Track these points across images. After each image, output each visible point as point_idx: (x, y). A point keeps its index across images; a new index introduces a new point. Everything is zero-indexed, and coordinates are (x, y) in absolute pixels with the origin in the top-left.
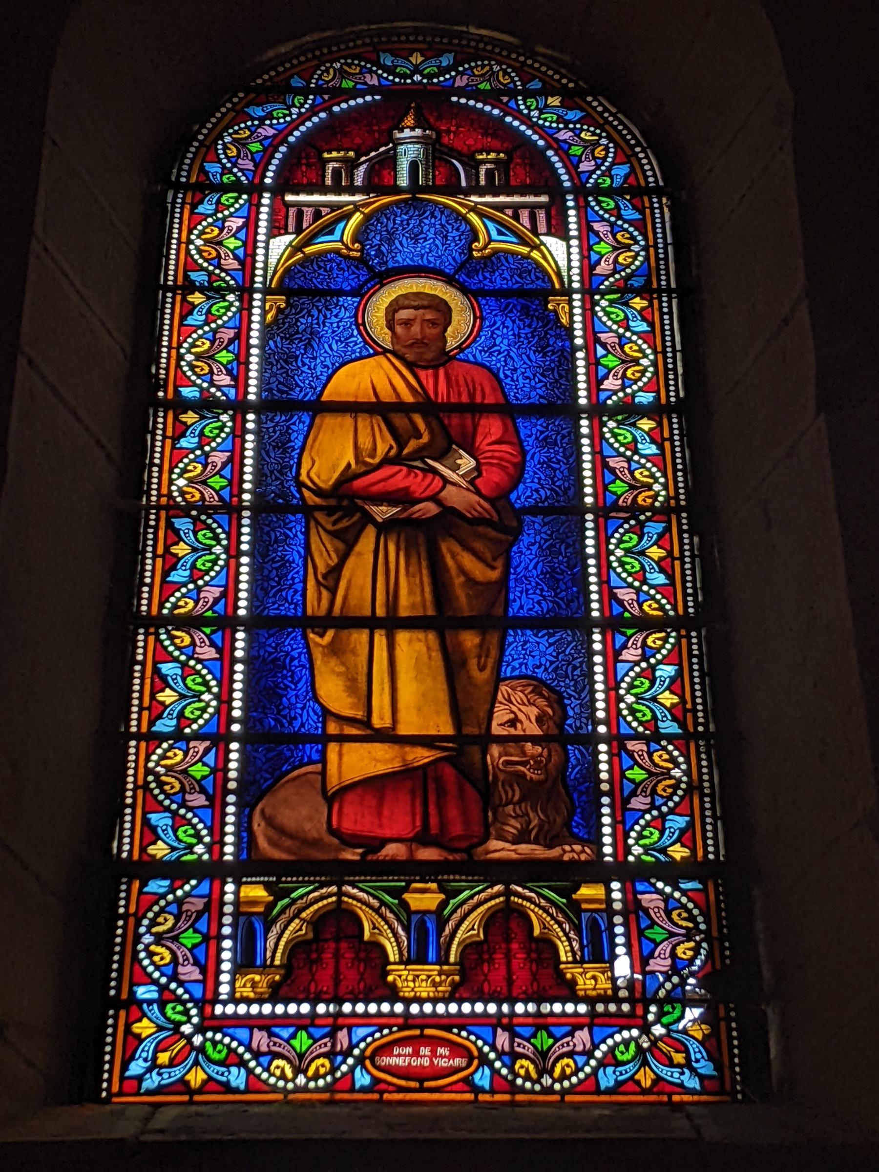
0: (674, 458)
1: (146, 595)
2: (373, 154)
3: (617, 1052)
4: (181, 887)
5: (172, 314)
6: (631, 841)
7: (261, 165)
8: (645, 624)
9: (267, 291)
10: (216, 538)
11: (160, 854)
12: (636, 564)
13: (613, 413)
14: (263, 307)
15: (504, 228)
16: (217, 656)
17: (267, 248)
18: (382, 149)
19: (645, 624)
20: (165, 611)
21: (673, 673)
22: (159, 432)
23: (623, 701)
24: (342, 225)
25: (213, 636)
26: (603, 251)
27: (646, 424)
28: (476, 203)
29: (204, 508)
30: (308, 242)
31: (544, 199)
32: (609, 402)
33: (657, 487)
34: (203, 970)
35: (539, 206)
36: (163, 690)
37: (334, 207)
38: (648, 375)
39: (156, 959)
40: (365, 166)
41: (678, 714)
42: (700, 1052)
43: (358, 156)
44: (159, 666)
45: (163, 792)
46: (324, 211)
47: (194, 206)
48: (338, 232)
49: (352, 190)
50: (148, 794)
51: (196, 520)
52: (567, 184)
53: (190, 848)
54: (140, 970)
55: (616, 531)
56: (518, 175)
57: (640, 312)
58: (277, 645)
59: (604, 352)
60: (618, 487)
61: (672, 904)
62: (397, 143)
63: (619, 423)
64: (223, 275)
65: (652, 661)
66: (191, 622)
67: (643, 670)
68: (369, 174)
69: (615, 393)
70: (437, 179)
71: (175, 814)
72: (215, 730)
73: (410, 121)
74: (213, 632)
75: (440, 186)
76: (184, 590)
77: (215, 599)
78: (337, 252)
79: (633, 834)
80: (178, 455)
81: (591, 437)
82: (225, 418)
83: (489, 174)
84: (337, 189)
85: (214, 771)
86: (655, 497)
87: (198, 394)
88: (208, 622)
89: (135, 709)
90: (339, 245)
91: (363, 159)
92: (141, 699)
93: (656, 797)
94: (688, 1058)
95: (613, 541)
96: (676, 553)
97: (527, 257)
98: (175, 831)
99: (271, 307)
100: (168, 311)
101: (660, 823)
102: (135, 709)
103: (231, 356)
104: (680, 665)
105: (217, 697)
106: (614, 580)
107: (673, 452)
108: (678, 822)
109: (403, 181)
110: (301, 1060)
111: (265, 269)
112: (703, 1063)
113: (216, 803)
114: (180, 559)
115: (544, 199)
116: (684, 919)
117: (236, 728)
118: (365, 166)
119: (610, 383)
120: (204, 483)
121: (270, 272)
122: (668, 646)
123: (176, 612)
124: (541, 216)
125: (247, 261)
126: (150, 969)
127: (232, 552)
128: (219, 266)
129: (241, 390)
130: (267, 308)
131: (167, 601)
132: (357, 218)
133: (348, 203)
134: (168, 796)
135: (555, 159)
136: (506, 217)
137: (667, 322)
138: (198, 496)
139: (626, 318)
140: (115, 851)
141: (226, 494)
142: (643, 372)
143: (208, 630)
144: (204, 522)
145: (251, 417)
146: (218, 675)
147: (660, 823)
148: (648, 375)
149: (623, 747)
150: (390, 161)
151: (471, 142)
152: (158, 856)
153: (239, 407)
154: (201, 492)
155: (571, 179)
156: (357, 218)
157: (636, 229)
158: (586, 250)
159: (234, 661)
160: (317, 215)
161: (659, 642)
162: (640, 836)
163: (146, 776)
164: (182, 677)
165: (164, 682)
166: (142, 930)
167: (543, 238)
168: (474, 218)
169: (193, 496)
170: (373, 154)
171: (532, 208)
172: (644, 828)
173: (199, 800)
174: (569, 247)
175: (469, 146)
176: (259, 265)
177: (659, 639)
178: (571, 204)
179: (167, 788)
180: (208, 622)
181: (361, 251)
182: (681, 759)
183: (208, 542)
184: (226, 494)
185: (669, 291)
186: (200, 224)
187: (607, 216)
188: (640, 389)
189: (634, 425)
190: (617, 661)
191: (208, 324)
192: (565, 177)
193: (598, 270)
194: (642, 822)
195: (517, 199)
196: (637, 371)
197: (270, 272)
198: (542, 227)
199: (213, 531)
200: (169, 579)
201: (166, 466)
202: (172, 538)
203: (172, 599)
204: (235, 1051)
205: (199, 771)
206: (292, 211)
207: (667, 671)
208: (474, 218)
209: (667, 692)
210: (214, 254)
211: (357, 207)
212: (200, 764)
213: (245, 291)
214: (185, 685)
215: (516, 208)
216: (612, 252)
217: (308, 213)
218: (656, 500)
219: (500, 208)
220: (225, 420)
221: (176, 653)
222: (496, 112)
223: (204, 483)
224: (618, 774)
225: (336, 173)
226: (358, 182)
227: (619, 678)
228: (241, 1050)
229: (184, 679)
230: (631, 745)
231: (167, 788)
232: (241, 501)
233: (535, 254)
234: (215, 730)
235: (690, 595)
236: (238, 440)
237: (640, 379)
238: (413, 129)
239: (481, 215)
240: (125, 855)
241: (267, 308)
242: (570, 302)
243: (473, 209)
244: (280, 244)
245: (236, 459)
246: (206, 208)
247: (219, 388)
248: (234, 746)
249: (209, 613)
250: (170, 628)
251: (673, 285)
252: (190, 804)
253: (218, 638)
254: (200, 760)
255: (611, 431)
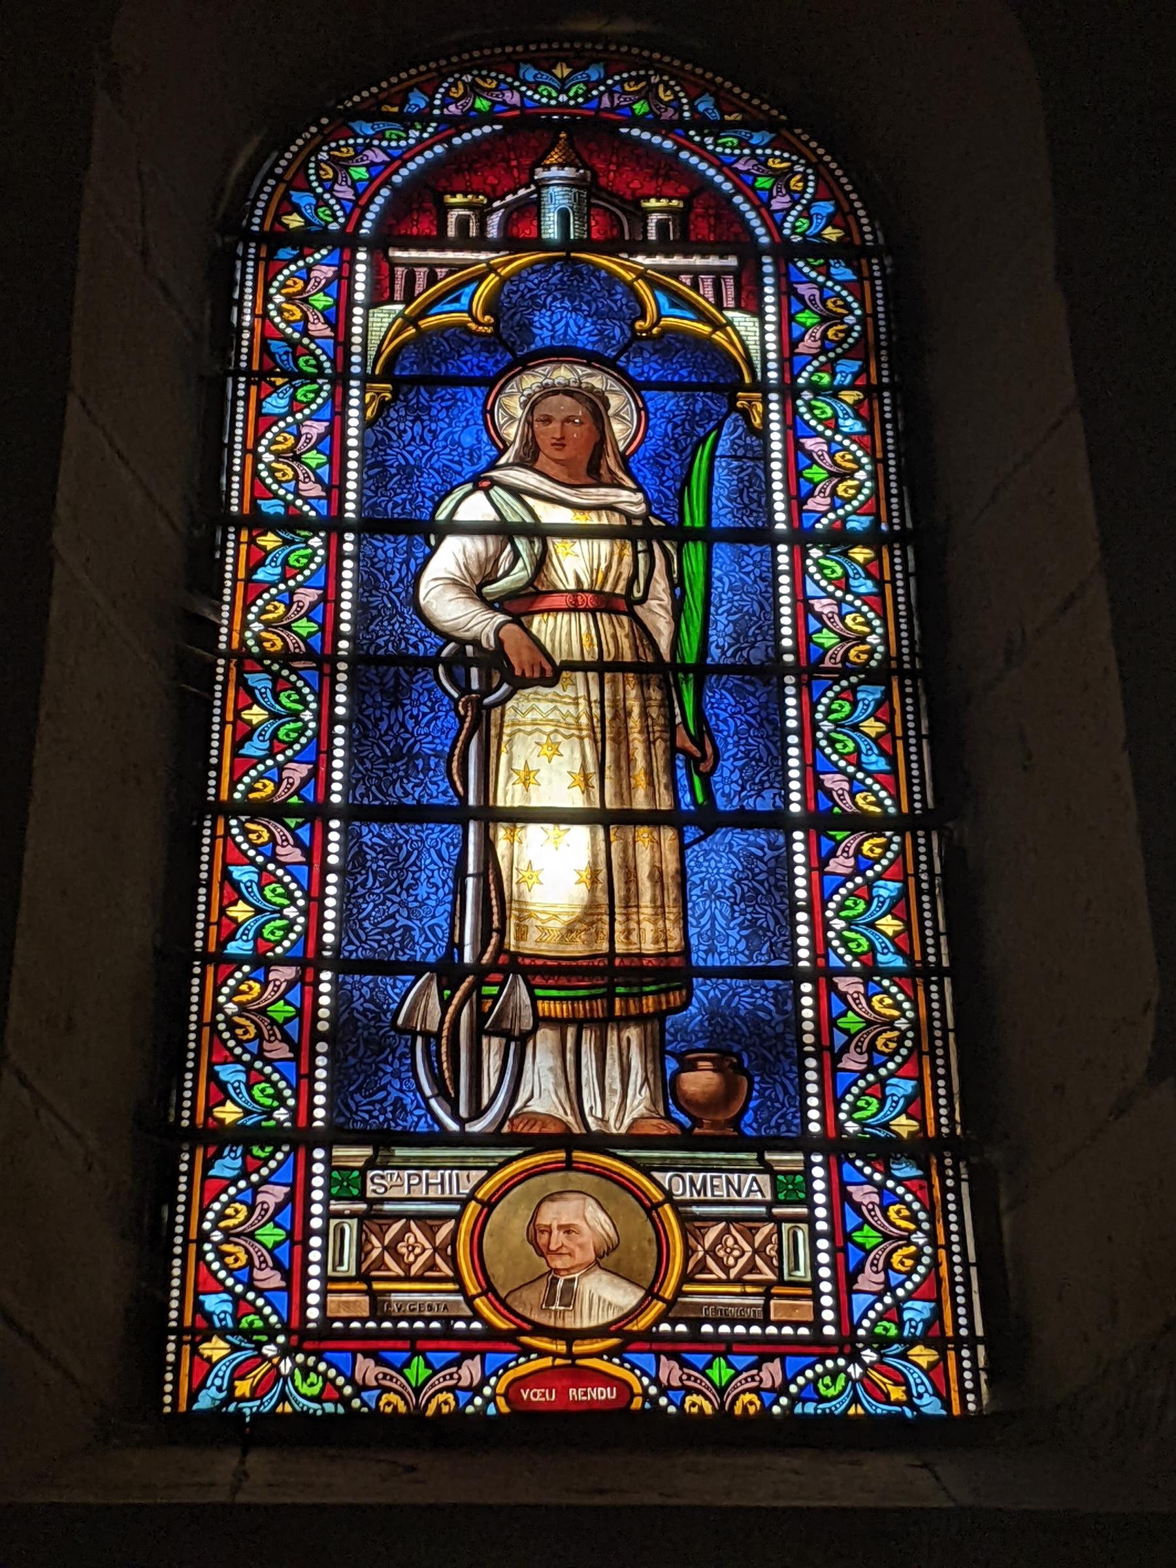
0: (896, 604)
1: (189, 1084)
2: (509, 198)
3: (820, 1385)
4: (312, 255)
5: (236, 557)
6: (819, 716)
7: (358, 208)
8: (860, 823)
9: (366, 379)
10: (303, 701)
11: (229, 1119)
12: (863, 941)
13: (816, 539)
14: (362, 398)
15: (678, 300)
16: (291, 1055)
17: (365, 326)
18: (522, 192)
19: (860, 823)
20: (237, 796)
21: (910, 1090)
22: (238, 446)
23: (820, 729)
24: (468, 290)
25: (298, 831)
26: (817, 478)
27: (860, 554)
28: (647, 267)
29: (286, 657)
30: (424, 313)
31: (732, 261)
32: (818, 526)
33: (873, 639)
34: (287, 1275)
35: (725, 271)
36: (250, 707)
37: (454, 268)
38: (866, 491)
39: (229, 1260)
40: (500, 213)
41: (900, 944)
42: (923, 1383)
43: (491, 201)
44: (231, 868)
45: (234, 1036)
46: (441, 272)
47: (208, 1165)
48: (465, 300)
49: (481, 243)
50: (216, 1039)
51: (276, 677)
52: (765, 240)
53: (269, 1113)
54: (228, 971)
55: (824, 695)
56: (701, 229)
57: (864, 566)
58: (383, 903)
59: (819, 626)
60: (826, 639)
61: (827, 293)
62: (542, 185)
63: (826, 551)
64: (280, 872)
65: (900, 1292)
66: (274, 811)
67: (857, 887)
68: (505, 225)
69: (824, 514)
70: (594, 229)
71: (262, 869)
72: (301, 954)
73: (555, 157)
74: (299, 826)
75: (597, 241)
76: (273, 591)
77: (277, 1204)
78: (463, 326)
79: (821, 708)
80: (254, 590)
81: (791, 573)
82: (315, 542)
83: (662, 226)
84: (463, 242)
85: (300, 1012)
86: (871, 652)
87: (281, 510)
88: (293, 811)
89: (200, 926)
90: (465, 317)
91: (497, 204)
92: (207, 912)
93: (875, 1054)
94: (908, 1392)
95: (832, 905)
96: (899, 732)
97: (708, 339)
98: (261, 890)
99: (373, 398)
100: (249, 284)
101: (879, 1090)
102: (207, 841)
103: (280, 1235)
104: (905, 882)
105: (304, 912)
106: (811, 590)
107: (895, 596)
108: (902, 1088)
109: (551, 230)
110: (417, 1395)
111: (364, 354)
112: (927, 1399)
113: (303, 1054)
114: (239, 925)
115: (732, 261)
116: (904, 1218)
117: (344, 644)
118: (500, 213)
119: (817, 503)
120: (288, 627)
121: (372, 353)
122: (890, 855)
123: (251, 796)
124: (729, 282)
125: (343, 343)
126: (222, 1274)
127: (326, 718)
128: (250, 1286)
129: (335, 504)
130: (367, 399)
131: (254, 603)
132: (492, 280)
133: (478, 262)
134: (240, 1043)
135: (745, 207)
136: (683, 285)
137: (927, 906)
138: (279, 644)
139: (846, 575)
140: (235, 321)
141: (316, 642)
142: (859, 489)
143: (292, 822)
144: (273, 873)
145: (349, 536)
146: (305, 884)
147: (879, 1090)
148: (866, 491)
149: (833, 987)
150: (533, 208)
151: (636, 184)
152: (228, 1121)
153: (333, 526)
154: (279, 703)
155: (769, 233)
156: (492, 280)
157: (851, 294)
158: (786, 320)
159: (326, 869)
160: (432, 280)
161: (878, 851)
162: (855, 1108)
163: (214, 1014)
164: (258, 884)
165: (236, 892)
166: (251, 617)
167: (729, 314)
168: (642, 287)
169: (273, 645)
170: (509, 198)
171: (718, 275)
172: (858, 1097)
173: (280, 1051)
174: (763, 322)
175: (634, 190)
176: (356, 349)
177: (877, 846)
178: (768, 269)
179: (239, 1031)
180: (293, 811)
181: (496, 326)
182: (855, 305)
183: (268, 1102)
184: (316, 642)
185: (972, 1341)
186: (260, 597)
187: (842, 763)
188: (855, 512)
189: (845, 554)
190: (851, 1292)
191: (293, 414)
192: (760, 231)
193: (801, 348)
194: (855, 1090)
195: (697, 261)
196: (863, 652)
197: (372, 353)
198: (729, 301)
199: (298, 691)
200: (242, 752)
201: (239, 603)
202: (245, 698)
203: (231, 982)
204: (333, 1381)
205: (281, 1011)
206: (400, 271)
207: (887, 890)
208: (642, 287)
209: (889, 917)
210: (290, 473)
211: (492, 269)
212: (271, 1225)
213: (341, 379)
214: (252, 1097)
215: (695, 273)
216: (820, 324)
217: (421, 274)
218: (871, 658)
219: (675, 273)
220: (292, 915)
221: (252, 853)
222: (668, 144)
223: (288, 627)
224: (827, 1022)
225: (463, 223)
226: (493, 232)
227: (826, 896)
228: (340, 1381)
229: (249, 1088)
230: (843, 984)
231: (239, 1031)
232: (336, 648)
233: (719, 337)
234: (301, 954)
235: (889, 421)
236: (298, 1249)
237: (854, 497)
238: (561, 166)
239: (653, 284)
240: (185, 1123)
241: (367, 399)
242: (766, 402)
243: (642, 275)
244: (384, 318)
245: (330, 597)
246: (276, 404)
247: (306, 500)
248: (326, 975)
249: (294, 800)
250: (243, 818)
251: (980, 1332)
252: (268, 1055)
253: (304, 834)
254: (282, 997)
255: (816, 562)
